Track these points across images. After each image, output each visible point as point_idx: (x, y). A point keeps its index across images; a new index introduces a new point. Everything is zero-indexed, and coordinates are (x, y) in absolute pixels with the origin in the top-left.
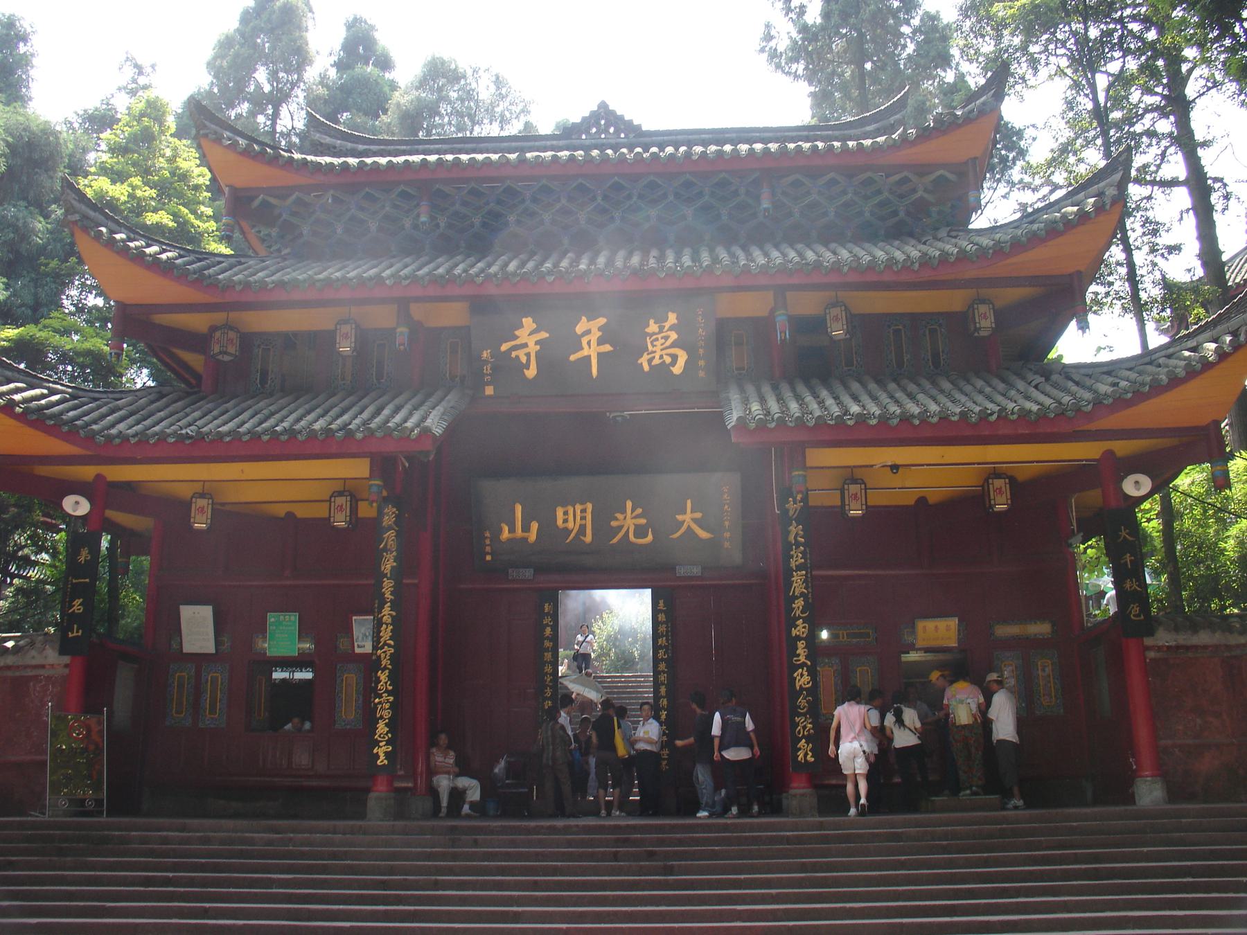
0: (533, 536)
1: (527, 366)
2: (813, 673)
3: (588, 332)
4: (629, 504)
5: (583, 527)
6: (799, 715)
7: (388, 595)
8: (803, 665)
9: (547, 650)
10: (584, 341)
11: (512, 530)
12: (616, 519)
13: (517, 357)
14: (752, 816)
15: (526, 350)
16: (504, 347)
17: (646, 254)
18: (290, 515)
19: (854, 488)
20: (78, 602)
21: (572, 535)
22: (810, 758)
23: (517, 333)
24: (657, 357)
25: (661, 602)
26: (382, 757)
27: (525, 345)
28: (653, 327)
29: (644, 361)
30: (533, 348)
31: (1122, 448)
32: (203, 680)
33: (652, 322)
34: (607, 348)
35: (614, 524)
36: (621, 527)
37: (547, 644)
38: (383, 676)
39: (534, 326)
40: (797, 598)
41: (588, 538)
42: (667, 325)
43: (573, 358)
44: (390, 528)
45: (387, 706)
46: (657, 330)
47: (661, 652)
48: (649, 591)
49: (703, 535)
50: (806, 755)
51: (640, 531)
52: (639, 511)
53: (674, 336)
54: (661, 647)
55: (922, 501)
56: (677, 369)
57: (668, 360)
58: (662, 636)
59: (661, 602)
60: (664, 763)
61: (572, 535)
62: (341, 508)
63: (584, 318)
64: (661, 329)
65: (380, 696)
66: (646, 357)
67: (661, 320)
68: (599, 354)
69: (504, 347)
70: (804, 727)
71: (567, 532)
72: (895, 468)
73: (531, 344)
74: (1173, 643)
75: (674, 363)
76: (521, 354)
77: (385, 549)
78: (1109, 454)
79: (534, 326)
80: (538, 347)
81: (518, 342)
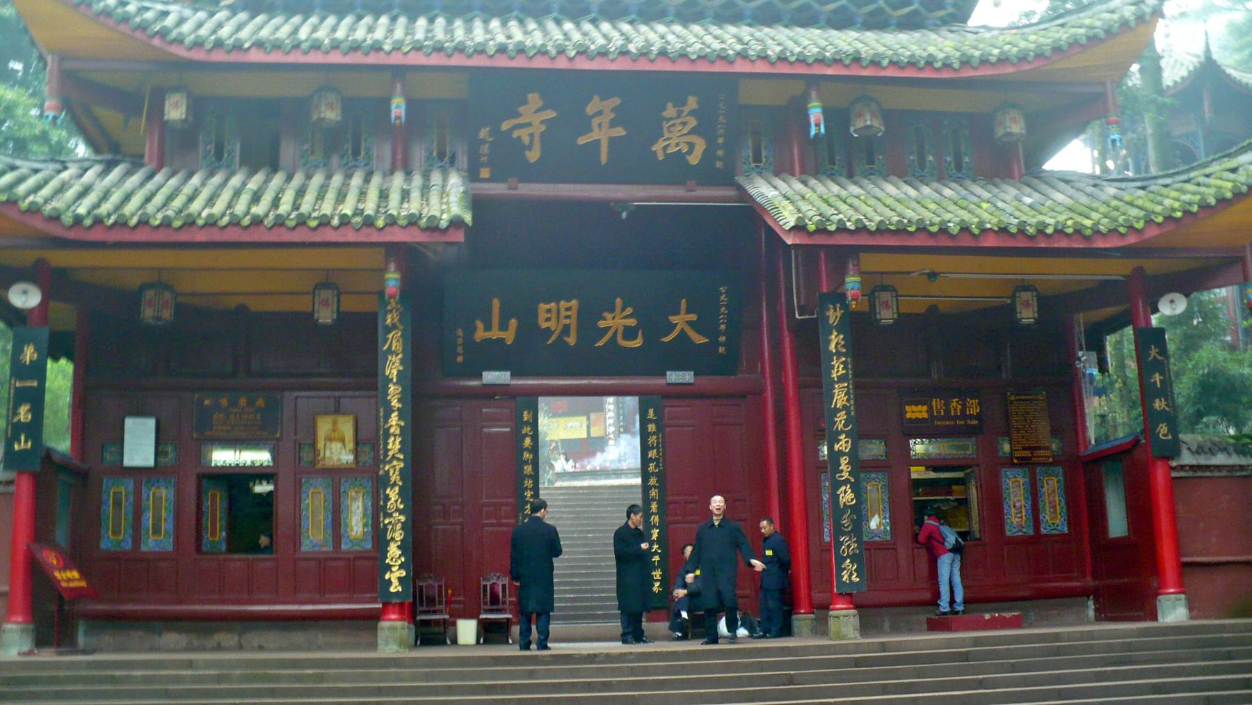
0: (509, 336)
1: (530, 148)
2: (856, 489)
3: (600, 113)
6: (844, 534)
7: (395, 403)
8: (846, 482)
9: (527, 463)
10: (595, 122)
11: (488, 327)
12: (604, 319)
14: (1089, 623)
15: (530, 130)
16: (505, 126)
18: (242, 309)
19: (886, 296)
21: (554, 338)
22: (855, 578)
23: (521, 109)
25: (651, 411)
26: (395, 582)
27: (529, 124)
28: (670, 111)
29: (657, 148)
31: (1151, 266)
32: (144, 496)
33: (670, 105)
34: (620, 132)
35: (602, 324)
36: (609, 328)
37: (527, 455)
38: (393, 494)
40: (839, 410)
41: (571, 340)
42: (686, 109)
43: (581, 141)
44: (394, 327)
45: (399, 526)
46: (675, 115)
47: (652, 467)
49: (700, 340)
50: (851, 574)
51: (629, 333)
53: (693, 122)
54: (651, 460)
55: (933, 309)
56: (694, 160)
58: (653, 448)
59: (651, 411)
60: (657, 584)
61: (554, 338)
62: (326, 303)
63: (596, 97)
65: (390, 515)
67: (681, 103)
68: (612, 141)
69: (505, 126)
70: (849, 546)
71: (548, 332)
72: (933, 275)
74: (1194, 462)
75: (690, 152)
76: (524, 135)
77: (390, 351)
78: (1140, 269)
80: (543, 128)
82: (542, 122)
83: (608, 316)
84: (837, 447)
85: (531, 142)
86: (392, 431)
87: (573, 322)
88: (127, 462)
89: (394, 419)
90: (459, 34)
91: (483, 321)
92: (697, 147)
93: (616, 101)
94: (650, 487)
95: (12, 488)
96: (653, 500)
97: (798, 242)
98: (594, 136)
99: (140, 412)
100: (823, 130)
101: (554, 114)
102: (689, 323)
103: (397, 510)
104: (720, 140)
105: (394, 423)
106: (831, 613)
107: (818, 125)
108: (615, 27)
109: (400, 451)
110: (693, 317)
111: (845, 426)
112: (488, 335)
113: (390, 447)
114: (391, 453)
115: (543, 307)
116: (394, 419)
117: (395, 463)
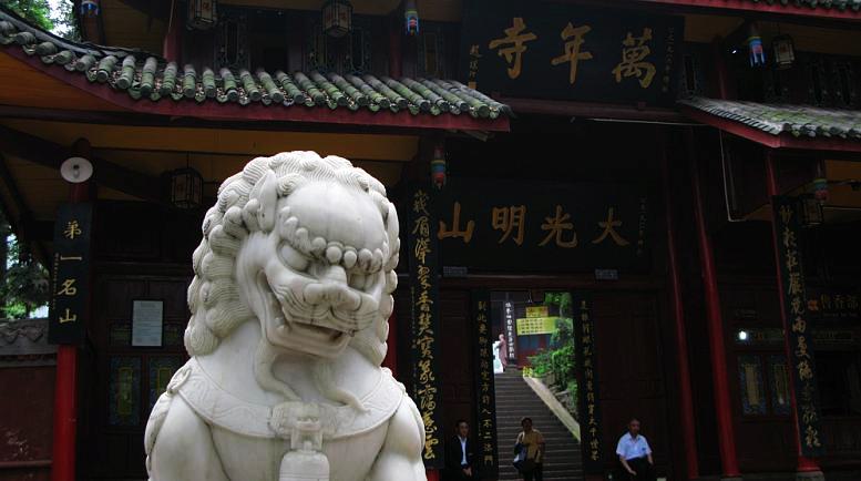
4: (559, 208)
5: (515, 229)
10: (568, 46)
11: (449, 229)
13: (504, 55)
15: (512, 50)
16: (492, 45)
17: (140, 60)
20: (68, 283)
21: (505, 236)
24: (630, 68)
27: (513, 45)
28: (630, 40)
29: (617, 72)
30: (520, 48)
33: (629, 35)
36: (550, 231)
39: (524, 27)
40: (795, 296)
41: (519, 241)
43: (554, 62)
44: (421, 213)
48: (159, 305)
49: (621, 242)
50: (813, 440)
51: (566, 236)
52: (567, 216)
53: (647, 51)
54: (585, 345)
56: (645, 83)
57: (639, 73)
64: (637, 42)
65: (423, 387)
66: (620, 68)
67: (638, 34)
68: (581, 63)
69: (492, 45)
70: (810, 415)
73: (519, 44)
75: (642, 77)
76: (508, 54)
77: (418, 235)
79: (524, 27)
81: (505, 41)
82: (524, 44)
83: (550, 220)
84: (794, 328)
85: (513, 62)
86: (422, 308)
87: (521, 225)
88: (135, 343)
89: (424, 298)
90: (189, 83)
91: (445, 222)
92: (648, 73)
93: (587, 29)
94: (585, 368)
95: (52, 362)
96: (589, 379)
97: (784, 145)
98: (566, 57)
99: (147, 296)
100: (763, 60)
101: (534, 37)
102: (614, 227)
103: (429, 382)
104: (668, 68)
105: (424, 301)
106: (799, 474)
107: (759, 56)
108: (311, 78)
109: (430, 327)
110: (619, 223)
111: (800, 310)
112: (449, 234)
113: (421, 323)
114: (422, 329)
115: (496, 211)
116: (424, 298)
117: (426, 338)
